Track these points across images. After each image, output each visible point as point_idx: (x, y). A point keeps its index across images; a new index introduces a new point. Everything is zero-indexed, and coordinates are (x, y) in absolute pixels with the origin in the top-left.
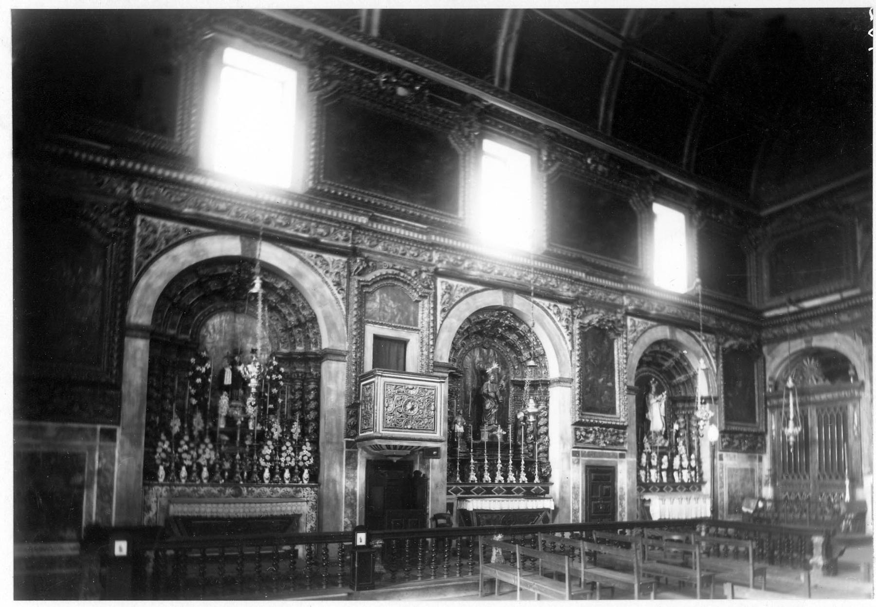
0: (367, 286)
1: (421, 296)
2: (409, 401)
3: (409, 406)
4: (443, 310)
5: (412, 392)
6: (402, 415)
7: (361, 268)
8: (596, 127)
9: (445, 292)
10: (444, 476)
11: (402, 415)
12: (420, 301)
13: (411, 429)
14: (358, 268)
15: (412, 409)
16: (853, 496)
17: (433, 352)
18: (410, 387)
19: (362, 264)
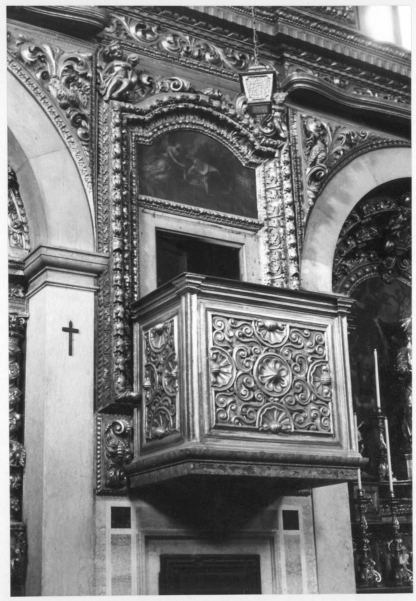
0: (144, 124)
1: (259, 154)
2: (268, 359)
3: (269, 372)
4: (314, 177)
5: (275, 338)
6: (256, 394)
7: (125, 84)
8: (152, 433)
9: (308, 548)
10: (351, 559)
11: (256, 394)
12: (257, 165)
13: (278, 431)
14: (119, 84)
15: (277, 380)
16: (92, 83)
17: (296, 275)
18: (269, 323)
19: (126, 76)
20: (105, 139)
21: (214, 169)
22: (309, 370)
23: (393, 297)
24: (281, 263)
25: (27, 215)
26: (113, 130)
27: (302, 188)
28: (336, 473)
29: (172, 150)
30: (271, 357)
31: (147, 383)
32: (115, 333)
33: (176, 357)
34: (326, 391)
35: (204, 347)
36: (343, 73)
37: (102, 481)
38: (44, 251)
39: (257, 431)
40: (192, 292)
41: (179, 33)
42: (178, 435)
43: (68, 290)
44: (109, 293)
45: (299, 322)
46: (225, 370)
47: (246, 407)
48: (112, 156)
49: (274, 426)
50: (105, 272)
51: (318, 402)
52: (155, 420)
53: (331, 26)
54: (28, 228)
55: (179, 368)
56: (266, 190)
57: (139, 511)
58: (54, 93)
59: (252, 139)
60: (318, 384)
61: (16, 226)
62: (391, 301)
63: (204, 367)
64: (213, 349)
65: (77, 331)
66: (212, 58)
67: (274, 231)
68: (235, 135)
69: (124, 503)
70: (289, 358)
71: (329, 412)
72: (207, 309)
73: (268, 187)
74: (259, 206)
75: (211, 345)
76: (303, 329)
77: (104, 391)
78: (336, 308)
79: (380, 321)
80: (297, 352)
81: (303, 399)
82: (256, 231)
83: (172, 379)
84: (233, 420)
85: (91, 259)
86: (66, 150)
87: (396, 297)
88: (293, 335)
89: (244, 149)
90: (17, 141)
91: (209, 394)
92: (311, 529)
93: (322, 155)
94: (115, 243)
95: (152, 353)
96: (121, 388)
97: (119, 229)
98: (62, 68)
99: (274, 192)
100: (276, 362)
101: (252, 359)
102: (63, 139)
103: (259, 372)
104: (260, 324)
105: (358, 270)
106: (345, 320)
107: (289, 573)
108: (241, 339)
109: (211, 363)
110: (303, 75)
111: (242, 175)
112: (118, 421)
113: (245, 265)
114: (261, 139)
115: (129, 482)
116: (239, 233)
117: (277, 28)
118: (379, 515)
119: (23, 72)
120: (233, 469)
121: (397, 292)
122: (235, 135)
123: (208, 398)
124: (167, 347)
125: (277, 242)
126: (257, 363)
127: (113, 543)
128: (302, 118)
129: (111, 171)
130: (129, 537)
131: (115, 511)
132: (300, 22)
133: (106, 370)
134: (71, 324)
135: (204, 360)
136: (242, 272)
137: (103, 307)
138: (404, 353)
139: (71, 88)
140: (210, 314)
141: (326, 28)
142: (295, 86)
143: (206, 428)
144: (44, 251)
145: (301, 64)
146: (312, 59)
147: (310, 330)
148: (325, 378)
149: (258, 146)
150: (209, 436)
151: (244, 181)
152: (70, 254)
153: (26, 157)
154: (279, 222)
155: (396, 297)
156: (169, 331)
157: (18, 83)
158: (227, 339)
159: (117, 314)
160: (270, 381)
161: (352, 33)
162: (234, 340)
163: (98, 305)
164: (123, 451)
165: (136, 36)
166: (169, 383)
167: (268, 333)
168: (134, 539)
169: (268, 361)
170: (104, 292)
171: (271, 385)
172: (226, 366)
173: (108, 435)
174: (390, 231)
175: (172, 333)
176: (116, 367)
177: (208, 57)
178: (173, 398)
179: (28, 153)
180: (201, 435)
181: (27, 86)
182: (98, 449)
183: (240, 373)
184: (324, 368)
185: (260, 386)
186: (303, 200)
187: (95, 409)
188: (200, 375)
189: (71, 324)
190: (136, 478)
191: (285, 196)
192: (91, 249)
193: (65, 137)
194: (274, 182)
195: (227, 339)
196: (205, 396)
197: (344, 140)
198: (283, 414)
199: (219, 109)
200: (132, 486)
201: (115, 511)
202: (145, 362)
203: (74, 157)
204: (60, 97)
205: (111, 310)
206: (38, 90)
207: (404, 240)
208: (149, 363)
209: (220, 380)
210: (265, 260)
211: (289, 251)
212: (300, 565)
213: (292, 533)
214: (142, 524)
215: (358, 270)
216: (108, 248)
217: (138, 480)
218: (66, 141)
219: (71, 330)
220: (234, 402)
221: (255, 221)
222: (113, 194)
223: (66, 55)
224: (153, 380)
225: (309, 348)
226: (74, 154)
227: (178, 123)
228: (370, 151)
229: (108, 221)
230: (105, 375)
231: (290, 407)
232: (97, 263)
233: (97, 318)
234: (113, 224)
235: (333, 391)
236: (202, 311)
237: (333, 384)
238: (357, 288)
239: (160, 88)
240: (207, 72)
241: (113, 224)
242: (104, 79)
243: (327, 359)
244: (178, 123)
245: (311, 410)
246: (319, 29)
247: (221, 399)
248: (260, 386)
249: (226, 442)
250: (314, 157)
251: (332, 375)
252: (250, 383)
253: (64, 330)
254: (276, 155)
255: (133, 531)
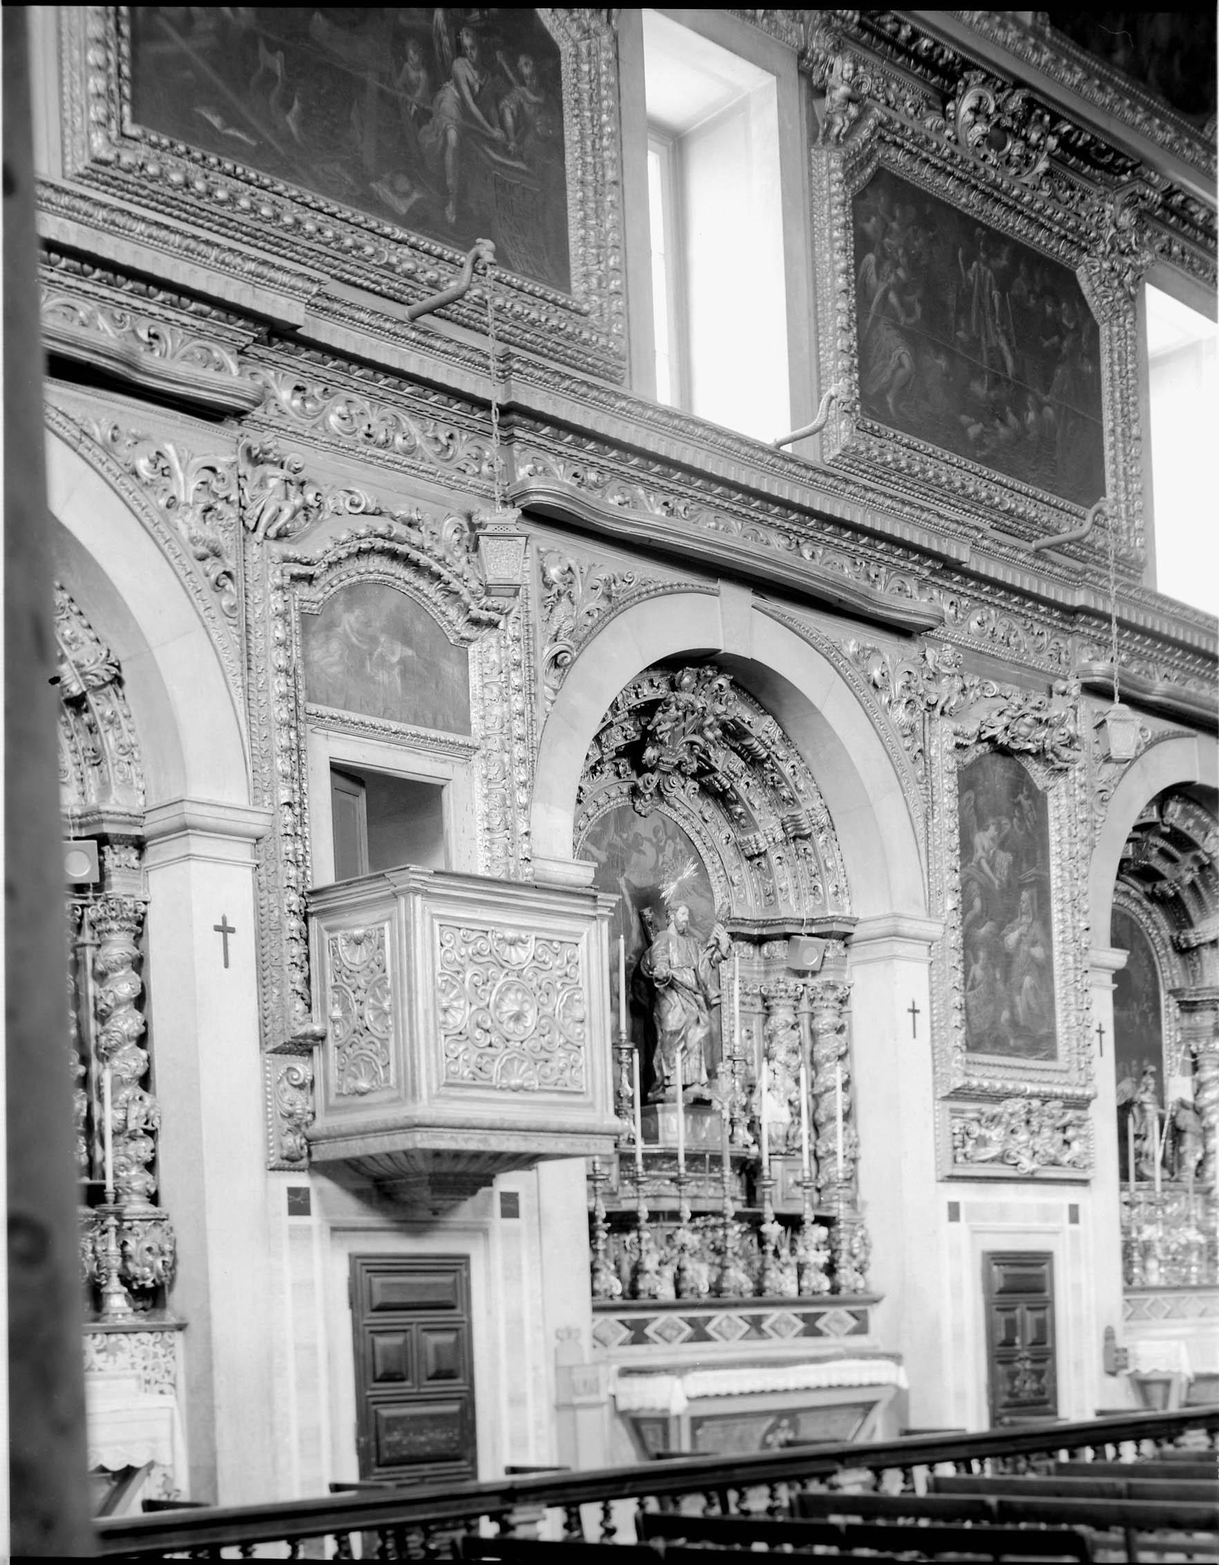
3: (510, 1007)
5: (518, 955)
6: (493, 1038)
11: (493, 1038)
15: (518, 1017)
18: (510, 934)
20: (259, 611)
21: (410, 652)
22: (558, 1001)
23: (650, 840)
24: (505, 813)
25: (138, 732)
26: (272, 597)
27: (535, 681)
28: (587, 1145)
29: (349, 620)
30: (512, 984)
31: (337, 1013)
32: (289, 935)
33: (389, 982)
34: (578, 1030)
35: (429, 972)
36: (602, 462)
37: (277, 1151)
38: (187, 807)
39: (494, 1088)
40: (416, 891)
41: (354, 397)
42: (394, 1094)
43: (218, 866)
44: (276, 872)
45: (546, 930)
46: (455, 1004)
47: (481, 1056)
48: (272, 643)
49: (515, 1082)
50: (267, 838)
51: (569, 1046)
52: (353, 1069)
53: (592, 387)
54: (139, 752)
55: (395, 999)
56: (484, 686)
57: (320, 1192)
58: (184, 533)
59: (467, 598)
60: (568, 1021)
61: (121, 750)
62: (646, 847)
63: (431, 1001)
64: (441, 974)
65: (232, 930)
66: (406, 443)
67: (496, 756)
68: (441, 589)
69: (301, 1180)
70: (534, 984)
71: (581, 1061)
72: (433, 916)
73: (486, 680)
74: (472, 714)
75: (438, 969)
76: (551, 941)
77: (273, 1021)
78: (595, 908)
79: (628, 881)
80: (544, 975)
81: (549, 1043)
82: (468, 759)
83: (382, 1014)
84: (466, 1074)
85: (250, 816)
86: (203, 630)
87: (654, 840)
88: (540, 951)
89: (452, 613)
90: (133, 618)
91: (437, 1039)
92: (536, 1218)
93: (569, 624)
94: (282, 793)
95: (344, 970)
96: (302, 1019)
97: (288, 769)
98: (194, 485)
99: (495, 690)
100: (518, 990)
101: (488, 987)
102: (197, 612)
103: (497, 1006)
104: (499, 935)
105: (598, 794)
106: (605, 925)
107: (506, 1278)
108: (476, 959)
109: (439, 995)
110: (546, 482)
111: (449, 659)
112: (294, 1066)
113: (452, 815)
114: (479, 599)
115: (310, 1154)
116: (445, 762)
117: (509, 390)
118: (617, 1198)
119: (137, 494)
120: (466, 1140)
121: (655, 832)
122: (441, 589)
123: (436, 1044)
124: (373, 965)
125: (499, 777)
126: (494, 992)
127: (291, 1237)
128: (539, 552)
129: (271, 670)
130: (309, 1229)
131: (293, 1192)
132: (546, 381)
133: (276, 991)
134: (224, 919)
135: (430, 991)
136: (446, 826)
137: (266, 893)
138: (664, 942)
139: (208, 523)
140: (437, 922)
141: (584, 389)
142: (531, 498)
143: (434, 1086)
144: (187, 807)
145: (539, 446)
146: (556, 439)
147: (561, 942)
148: (579, 1014)
149: (476, 612)
150: (439, 1096)
151: (450, 669)
152: (222, 810)
153: (147, 646)
154: (503, 743)
155: (654, 840)
156: (375, 942)
157: (129, 512)
158: (458, 959)
159: (289, 906)
160: (511, 1018)
161: (625, 398)
162: (467, 959)
163: (259, 887)
164: (304, 1109)
165: (292, 408)
166: (376, 1018)
167: (508, 948)
168: (316, 1232)
169: (508, 989)
170: (267, 869)
171: (511, 1024)
172: (457, 998)
173: (281, 1086)
174: (653, 733)
175: (380, 946)
176: (292, 986)
177: (399, 440)
178: (384, 1042)
179: (152, 639)
180: (429, 1095)
181: (105, 474)
182: (268, 1106)
183: (474, 1007)
184: (577, 997)
185: (498, 1025)
186: (537, 703)
187: (261, 1048)
188: (426, 1011)
189: (224, 919)
190: (321, 1147)
191: (513, 698)
192: (242, 800)
193: (201, 609)
194: (496, 672)
195: (458, 959)
196: (432, 1042)
197: (600, 591)
198: (526, 1064)
199: (420, 548)
200: (315, 1158)
201: (293, 1192)
202: (330, 982)
203: (215, 642)
204: (193, 540)
205: (279, 898)
206: (160, 526)
207: (674, 745)
208: (339, 983)
209: (450, 1020)
210: (481, 807)
211: (518, 793)
212: (519, 1267)
213: (511, 1222)
214: (326, 1211)
215: (598, 794)
216: (272, 798)
217: (323, 1152)
218: (203, 615)
219: (224, 929)
220: (466, 1049)
221: (469, 741)
222: (276, 710)
223: (200, 461)
224: (346, 1010)
225: (559, 968)
226: (215, 637)
227: (359, 573)
228: (637, 603)
229: (268, 754)
230: (275, 997)
231: (534, 1055)
232: (258, 823)
233: (259, 909)
234: (279, 761)
235: (587, 1030)
236: (427, 919)
237: (587, 1021)
238: (597, 825)
239: (332, 508)
240: (397, 470)
241: (279, 761)
242: (252, 500)
243: (580, 985)
244: (359, 573)
245: (560, 1059)
246: (573, 391)
247: (452, 1046)
248: (498, 1025)
249: (457, 1104)
250: (556, 628)
251: (586, 1008)
252: (485, 1022)
253: (217, 929)
254: (501, 625)
255: (315, 1220)
